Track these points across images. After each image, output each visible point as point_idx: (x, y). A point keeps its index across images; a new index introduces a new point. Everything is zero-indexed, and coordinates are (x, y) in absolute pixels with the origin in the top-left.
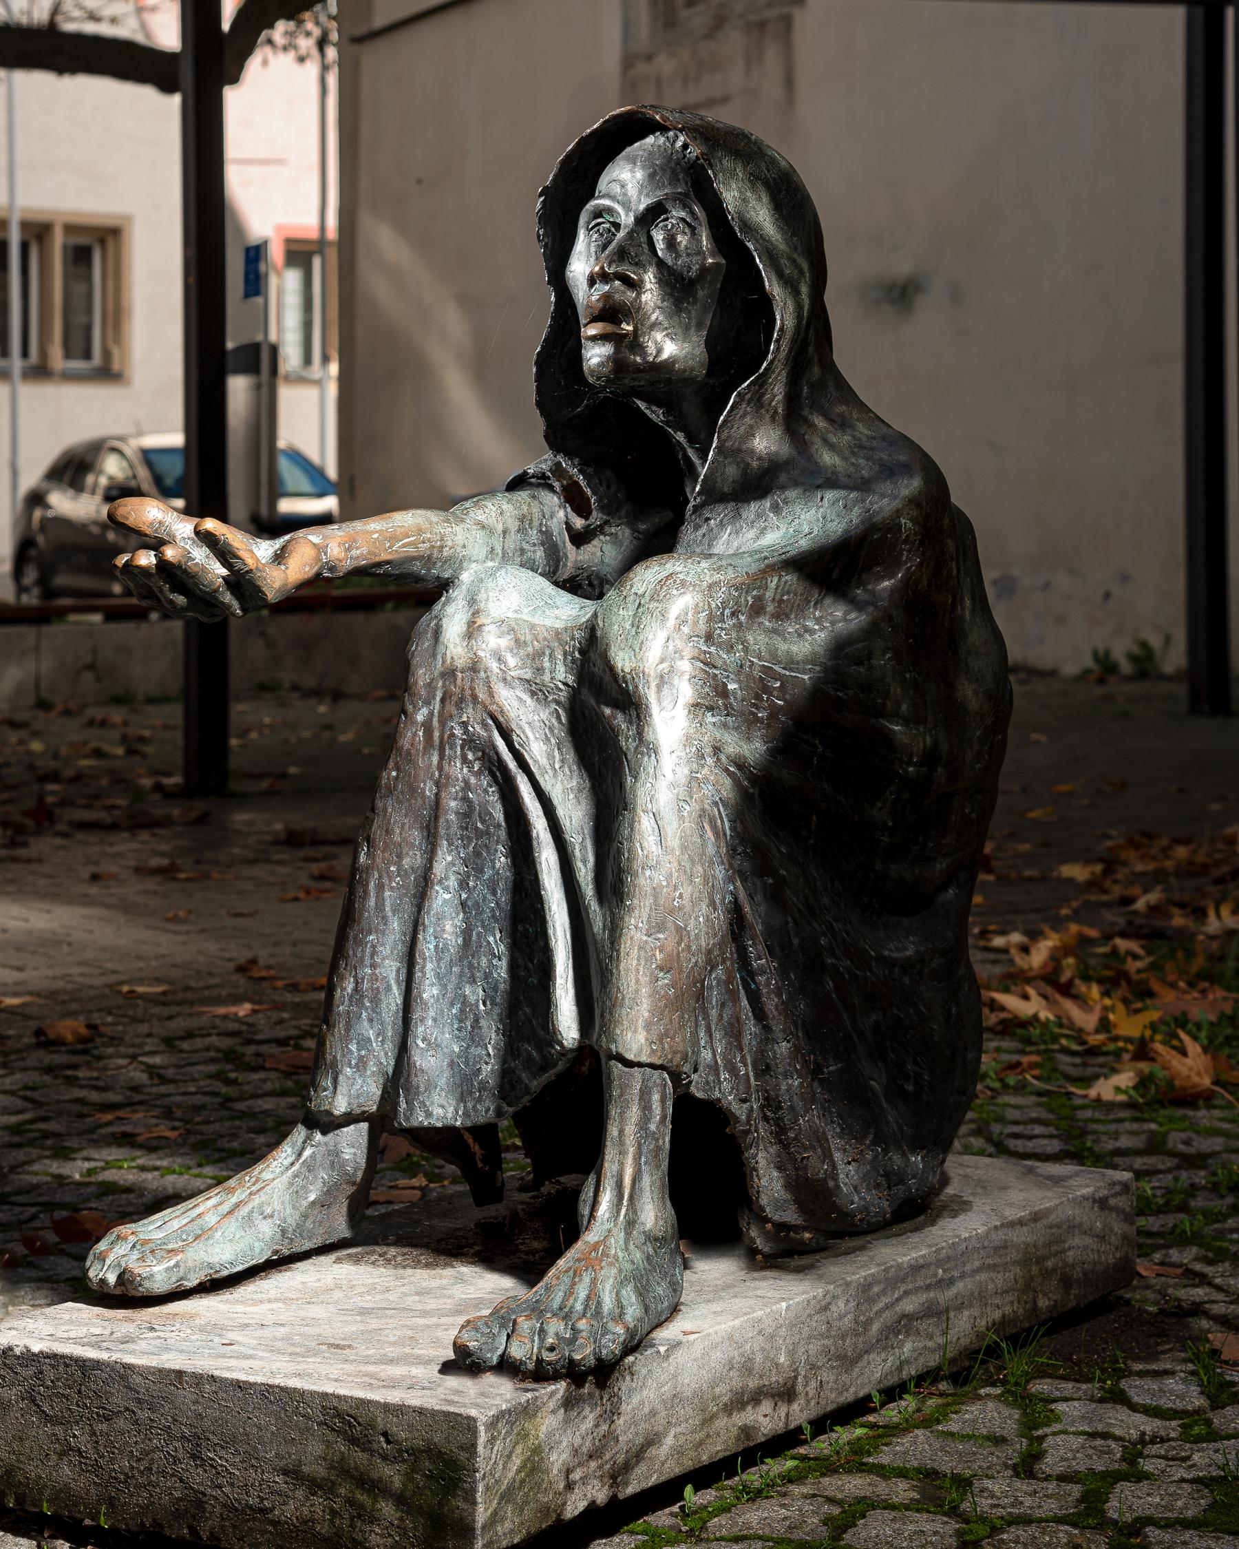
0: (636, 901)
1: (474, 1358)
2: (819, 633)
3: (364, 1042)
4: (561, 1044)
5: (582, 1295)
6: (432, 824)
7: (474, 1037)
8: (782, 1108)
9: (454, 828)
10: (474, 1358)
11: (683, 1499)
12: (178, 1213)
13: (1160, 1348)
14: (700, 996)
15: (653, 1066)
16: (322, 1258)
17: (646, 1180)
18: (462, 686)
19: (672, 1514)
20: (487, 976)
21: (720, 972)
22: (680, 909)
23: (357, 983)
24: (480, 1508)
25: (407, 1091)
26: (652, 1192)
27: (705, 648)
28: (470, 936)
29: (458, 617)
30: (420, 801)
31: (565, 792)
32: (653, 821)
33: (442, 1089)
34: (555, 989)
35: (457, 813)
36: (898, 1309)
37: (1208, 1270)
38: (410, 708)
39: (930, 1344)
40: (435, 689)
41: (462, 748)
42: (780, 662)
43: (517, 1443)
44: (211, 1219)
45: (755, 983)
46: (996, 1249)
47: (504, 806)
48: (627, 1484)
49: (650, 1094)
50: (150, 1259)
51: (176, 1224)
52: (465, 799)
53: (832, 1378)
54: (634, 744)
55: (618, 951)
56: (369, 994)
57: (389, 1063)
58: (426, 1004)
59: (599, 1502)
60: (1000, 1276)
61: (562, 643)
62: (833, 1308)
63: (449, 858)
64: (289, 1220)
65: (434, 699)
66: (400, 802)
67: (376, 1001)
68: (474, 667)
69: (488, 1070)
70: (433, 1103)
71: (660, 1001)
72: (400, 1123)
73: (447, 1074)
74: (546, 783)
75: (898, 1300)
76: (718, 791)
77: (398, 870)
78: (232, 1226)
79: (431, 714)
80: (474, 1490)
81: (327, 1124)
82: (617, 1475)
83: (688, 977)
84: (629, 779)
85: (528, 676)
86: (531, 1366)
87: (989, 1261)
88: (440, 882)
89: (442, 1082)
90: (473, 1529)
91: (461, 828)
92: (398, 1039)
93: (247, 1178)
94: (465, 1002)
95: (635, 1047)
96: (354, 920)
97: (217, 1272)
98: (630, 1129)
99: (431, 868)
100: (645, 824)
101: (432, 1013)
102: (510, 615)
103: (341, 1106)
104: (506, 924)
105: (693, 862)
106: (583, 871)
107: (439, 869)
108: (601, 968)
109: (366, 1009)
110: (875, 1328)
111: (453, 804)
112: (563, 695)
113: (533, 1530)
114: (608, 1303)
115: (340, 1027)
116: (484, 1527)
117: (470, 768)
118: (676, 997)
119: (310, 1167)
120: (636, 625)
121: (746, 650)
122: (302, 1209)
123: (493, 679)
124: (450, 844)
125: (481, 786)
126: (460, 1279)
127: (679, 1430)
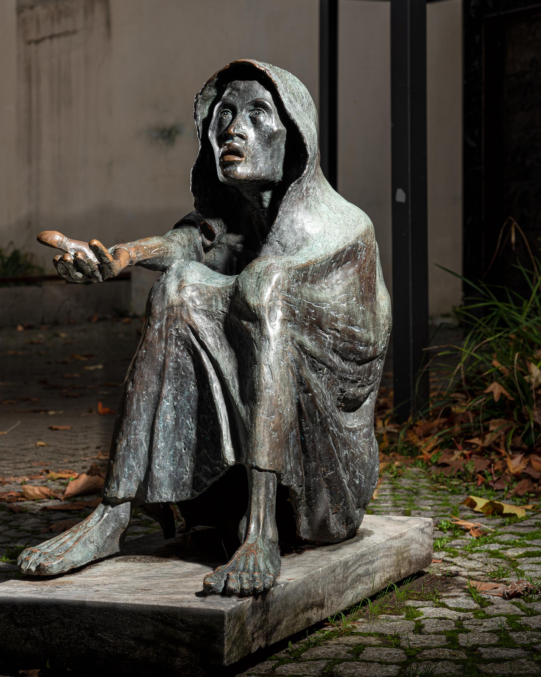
0: (262, 403)
1: (213, 589)
2: (327, 290)
3: (131, 468)
4: (227, 464)
5: (252, 564)
6: (162, 373)
7: (180, 463)
8: (310, 490)
9: (172, 374)
10: (213, 589)
11: (288, 646)
12: (53, 542)
13: (449, 588)
14: (287, 442)
15: (271, 471)
16: (109, 561)
17: (268, 519)
18: (176, 313)
19: (284, 653)
20: (186, 437)
21: (294, 432)
22: (281, 405)
23: (128, 442)
24: (226, 647)
25: (152, 487)
26: (271, 523)
27: (287, 295)
28: (179, 421)
29: (173, 283)
30: (156, 363)
31: (224, 358)
32: (268, 369)
33: (166, 486)
34: (223, 441)
35: (173, 368)
36: (357, 572)
37: (452, 560)
38: (152, 323)
39: (366, 587)
40: (164, 314)
41: (176, 340)
42: (314, 302)
43: (237, 622)
44: (70, 544)
45: (304, 437)
46: (388, 548)
47: (194, 364)
48: (271, 640)
49: (269, 483)
50: (50, 560)
51: (55, 546)
52: (176, 362)
53: (336, 600)
54: (259, 337)
55: (255, 424)
56: (133, 446)
57: (142, 476)
58: (159, 450)
59: (262, 646)
60: (389, 559)
61: (221, 294)
62: (336, 571)
63: (169, 388)
64: (100, 544)
65: (163, 319)
66: (147, 364)
67: (136, 449)
68: (182, 304)
69: (187, 478)
70: (162, 492)
71: (273, 444)
72: (148, 501)
73: (168, 480)
74: (215, 354)
75: (357, 568)
76: (293, 356)
77: (146, 393)
78: (79, 546)
79: (162, 325)
80: (223, 640)
81: (114, 502)
82: (268, 636)
83: (284, 434)
84: (257, 351)
85: (206, 308)
86: (238, 591)
87: (386, 553)
88: (165, 398)
89: (166, 483)
90: (223, 656)
91: (175, 374)
92: (146, 466)
93: (81, 527)
94: (176, 449)
95: (263, 463)
96: (126, 415)
97: (76, 565)
98: (261, 497)
99: (161, 392)
100: (266, 370)
101: (162, 454)
102: (197, 282)
103: (121, 494)
104: (195, 415)
105: (285, 385)
106: (234, 391)
107: (165, 392)
108: (246, 430)
109: (132, 453)
110: (349, 579)
111: (171, 364)
112: (221, 317)
113: (242, 657)
114: (262, 567)
115: (120, 461)
116: (227, 655)
117: (179, 349)
118: (279, 442)
119: (107, 521)
120: (259, 286)
121: (302, 296)
122: (104, 539)
123: (190, 310)
124: (170, 381)
125: (183, 356)
126: (176, 566)
127: (287, 619)
